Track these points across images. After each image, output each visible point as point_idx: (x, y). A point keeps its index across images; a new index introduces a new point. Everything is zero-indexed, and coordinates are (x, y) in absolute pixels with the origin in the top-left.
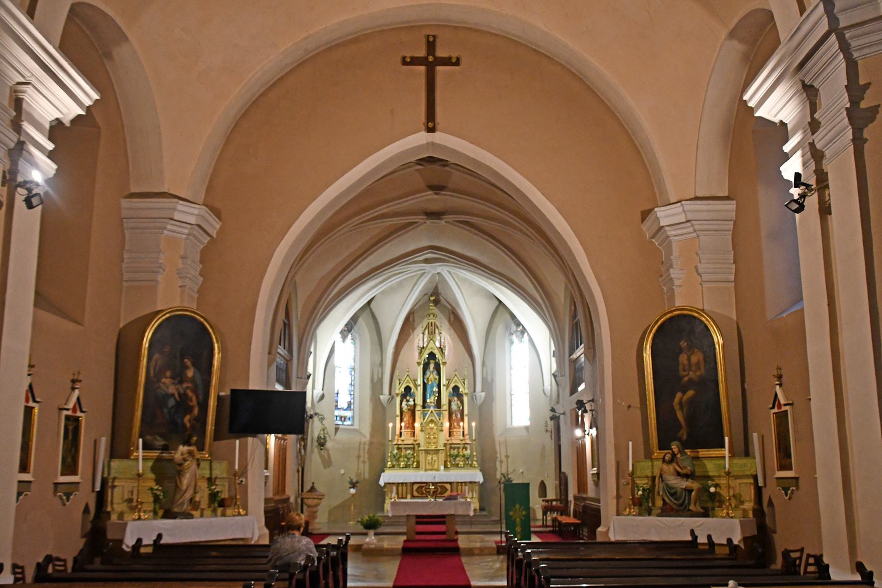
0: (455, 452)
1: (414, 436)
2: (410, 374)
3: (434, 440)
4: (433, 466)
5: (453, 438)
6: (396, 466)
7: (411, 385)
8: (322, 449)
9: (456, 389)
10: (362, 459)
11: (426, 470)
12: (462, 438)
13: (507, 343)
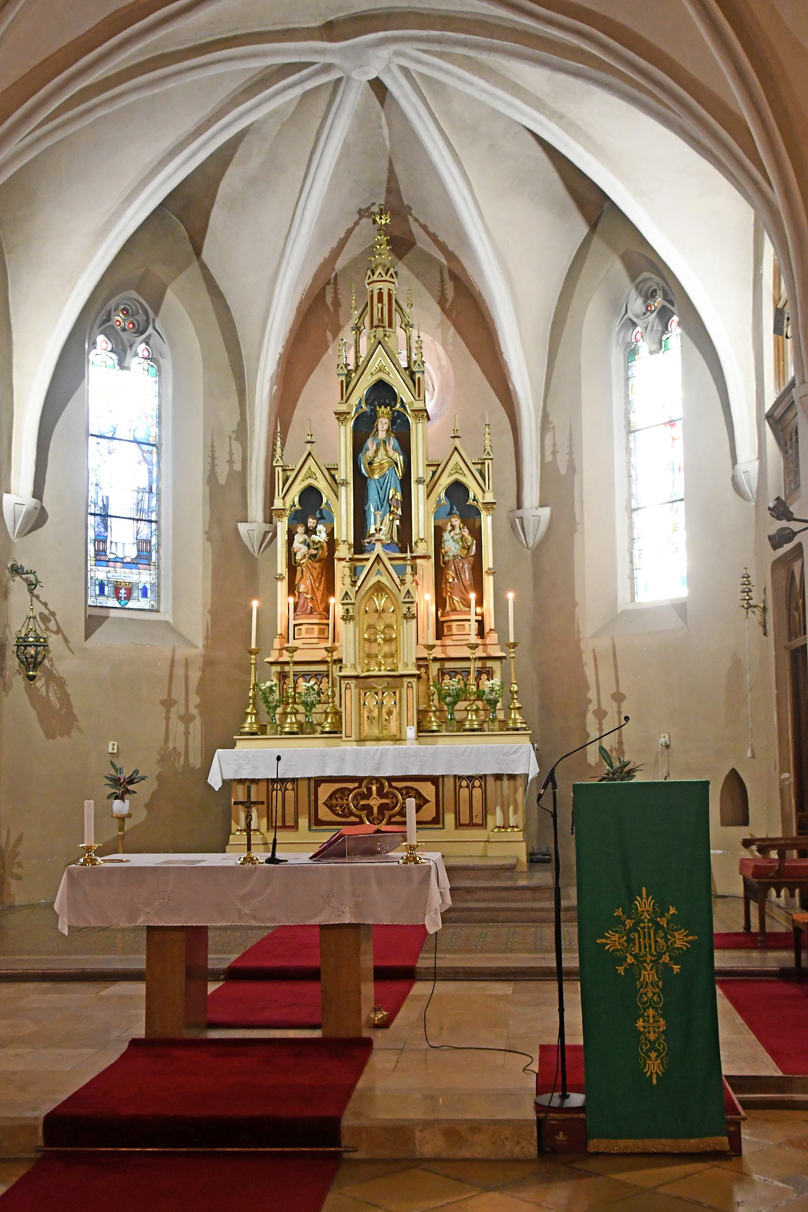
0: (451, 684)
3: (386, 648)
4: (383, 728)
5: (448, 641)
7: (321, 484)
8: (32, 678)
9: (457, 490)
10: (178, 710)
11: (361, 740)
12: (474, 639)
13: (616, 355)
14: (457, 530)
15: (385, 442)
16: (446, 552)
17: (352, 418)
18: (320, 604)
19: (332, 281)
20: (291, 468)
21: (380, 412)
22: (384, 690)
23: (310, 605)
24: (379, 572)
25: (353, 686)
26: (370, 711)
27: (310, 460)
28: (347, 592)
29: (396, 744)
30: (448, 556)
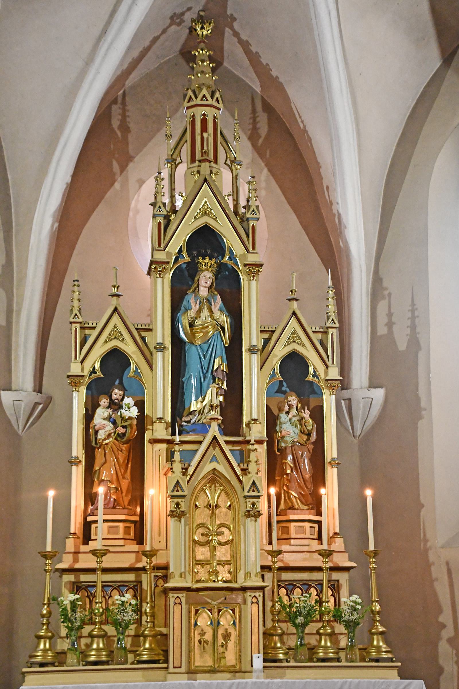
1: (140, 539)
2: (122, 304)
6: (72, 659)
11: (191, 672)
14: (294, 412)
15: (208, 301)
16: (283, 437)
17: (171, 269)
18: (126, 496)
19: (120, 100)
20: (90, 325)
21: (204, 264)
22: (221, 607)
23: (114, 497)
24: (214, 459)
25: (183, 600)
26: (203, 634)
27: (116, 317)
28: (178, 482)
29: (235, 677)
30: (286, 442)
